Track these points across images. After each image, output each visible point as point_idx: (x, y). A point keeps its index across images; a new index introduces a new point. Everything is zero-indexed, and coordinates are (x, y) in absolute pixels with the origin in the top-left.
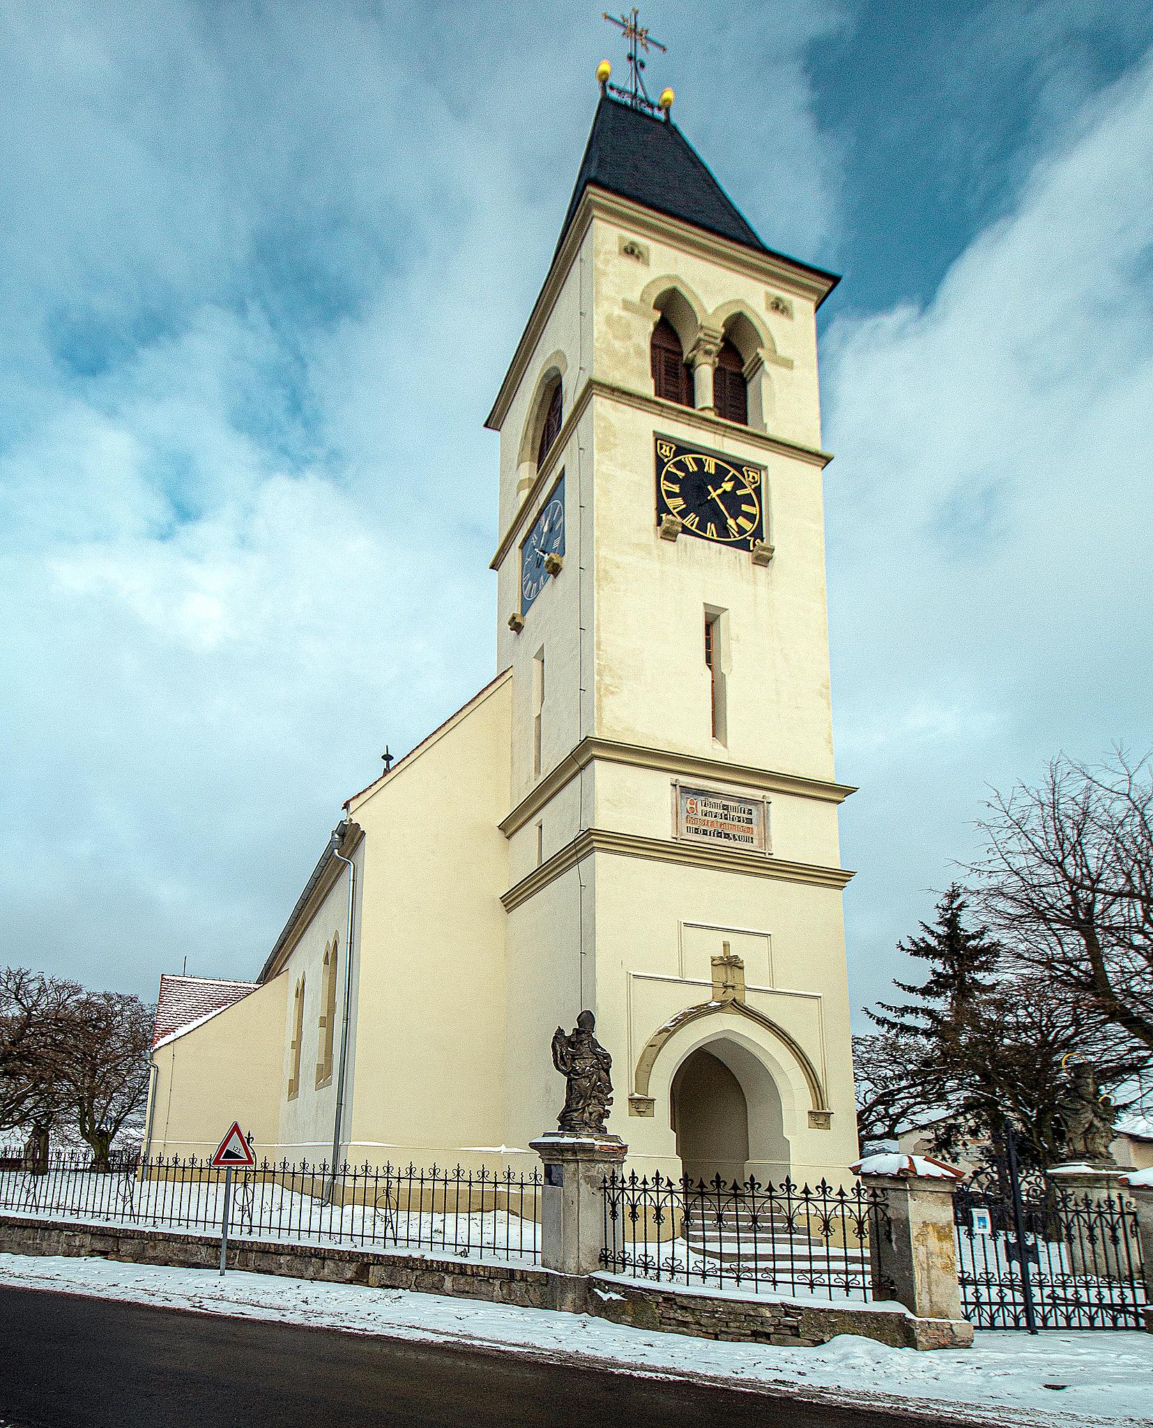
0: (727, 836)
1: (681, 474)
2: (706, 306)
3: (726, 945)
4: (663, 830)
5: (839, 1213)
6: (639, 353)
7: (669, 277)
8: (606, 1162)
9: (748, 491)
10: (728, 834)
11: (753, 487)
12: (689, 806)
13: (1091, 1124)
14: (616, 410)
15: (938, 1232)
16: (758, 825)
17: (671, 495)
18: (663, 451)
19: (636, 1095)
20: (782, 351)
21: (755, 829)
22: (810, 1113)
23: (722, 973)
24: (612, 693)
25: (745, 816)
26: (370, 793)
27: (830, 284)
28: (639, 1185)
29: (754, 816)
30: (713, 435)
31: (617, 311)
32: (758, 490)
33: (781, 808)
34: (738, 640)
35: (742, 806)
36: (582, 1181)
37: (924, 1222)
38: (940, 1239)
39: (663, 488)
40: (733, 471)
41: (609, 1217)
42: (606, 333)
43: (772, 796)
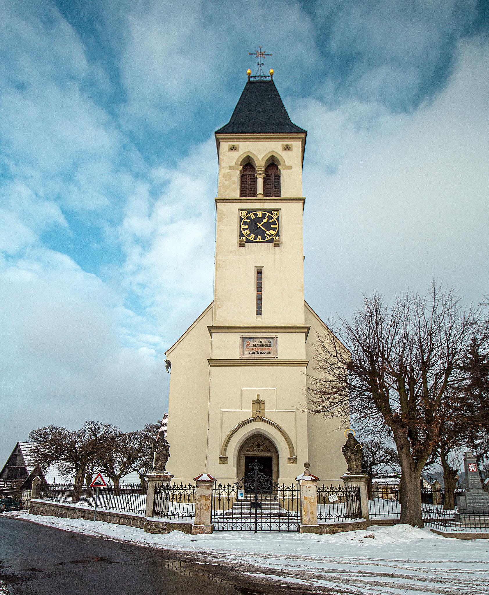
0: (261, 353)
1: (249, 221)
2: (259, 158)
3: (258, 395)
4: (236, 355)
5: (184, 494)
6: (234, 183)
7: (246, 153)
8: (159, 481)
9: (274, 219)
10: (262, 352)
11: (276, 217)
12: (247, 344)
13: (349, 456)
14: (225, 205)
15: (205, 498)
16: (273, 347)
17: (244, 230)
18: (242, 215)
19: (221, 456)
20: (287, 164)
21: (272, 348)
22: (288, 458)
23: (257, 407)
24: (220, 308)
25: (269, 344)
26: (173, 348)
27: (305, 134)
28: (176, 488)
29: (272, 344)
30: (260, 203)
31: (227, 171)
32: (278, 219)
33: (282, 338)
34: (267, 277)
35: (268, 340)
36: (151, 487)
37: (201, 495)
38: (206, 500)
39: (242, 228)
40: (268, 214)
41: (351, 501)
42: (223, 180)
43: (279, 335)
